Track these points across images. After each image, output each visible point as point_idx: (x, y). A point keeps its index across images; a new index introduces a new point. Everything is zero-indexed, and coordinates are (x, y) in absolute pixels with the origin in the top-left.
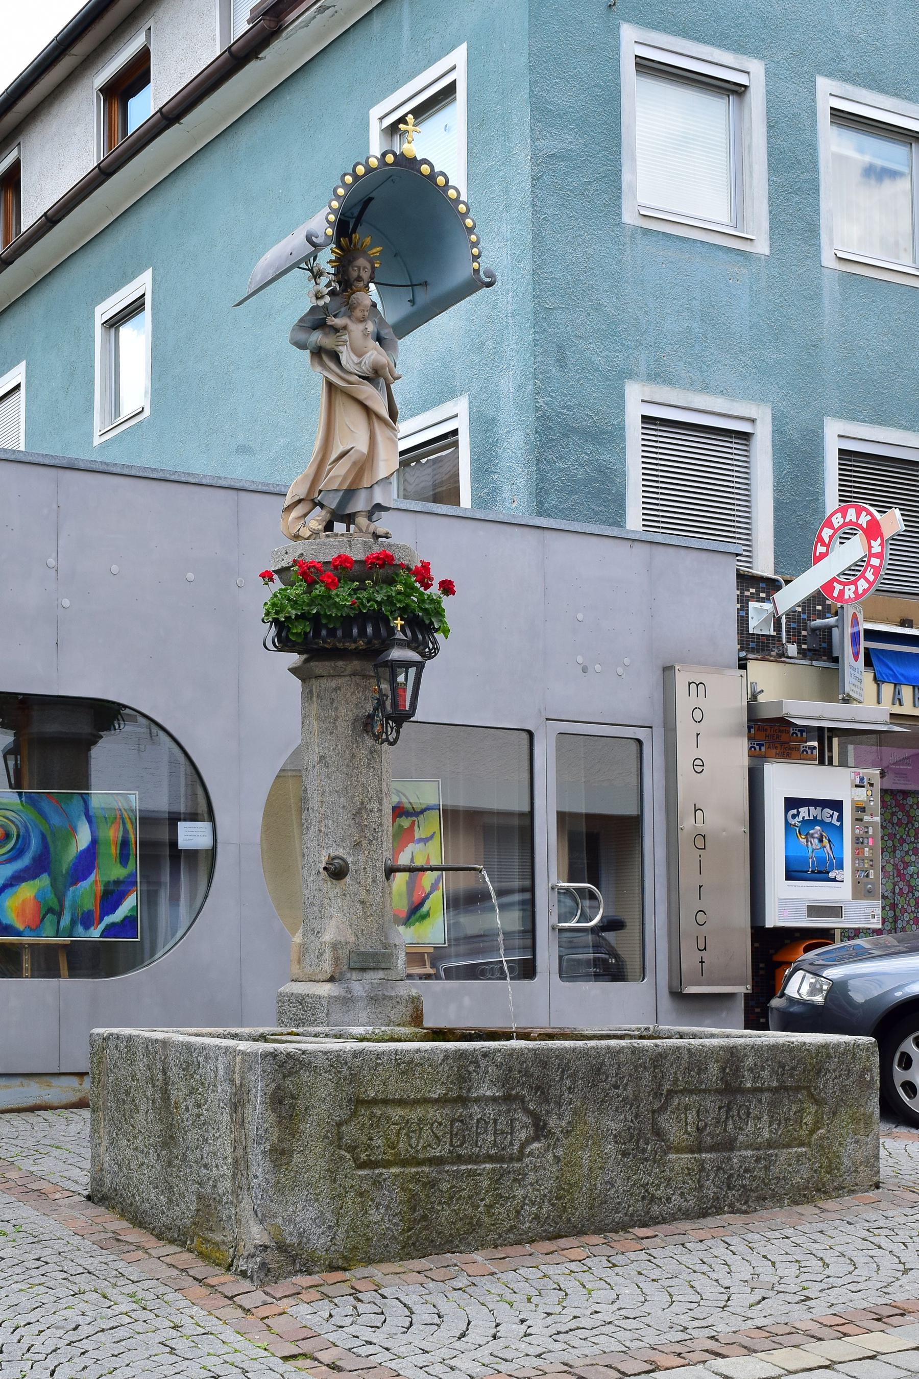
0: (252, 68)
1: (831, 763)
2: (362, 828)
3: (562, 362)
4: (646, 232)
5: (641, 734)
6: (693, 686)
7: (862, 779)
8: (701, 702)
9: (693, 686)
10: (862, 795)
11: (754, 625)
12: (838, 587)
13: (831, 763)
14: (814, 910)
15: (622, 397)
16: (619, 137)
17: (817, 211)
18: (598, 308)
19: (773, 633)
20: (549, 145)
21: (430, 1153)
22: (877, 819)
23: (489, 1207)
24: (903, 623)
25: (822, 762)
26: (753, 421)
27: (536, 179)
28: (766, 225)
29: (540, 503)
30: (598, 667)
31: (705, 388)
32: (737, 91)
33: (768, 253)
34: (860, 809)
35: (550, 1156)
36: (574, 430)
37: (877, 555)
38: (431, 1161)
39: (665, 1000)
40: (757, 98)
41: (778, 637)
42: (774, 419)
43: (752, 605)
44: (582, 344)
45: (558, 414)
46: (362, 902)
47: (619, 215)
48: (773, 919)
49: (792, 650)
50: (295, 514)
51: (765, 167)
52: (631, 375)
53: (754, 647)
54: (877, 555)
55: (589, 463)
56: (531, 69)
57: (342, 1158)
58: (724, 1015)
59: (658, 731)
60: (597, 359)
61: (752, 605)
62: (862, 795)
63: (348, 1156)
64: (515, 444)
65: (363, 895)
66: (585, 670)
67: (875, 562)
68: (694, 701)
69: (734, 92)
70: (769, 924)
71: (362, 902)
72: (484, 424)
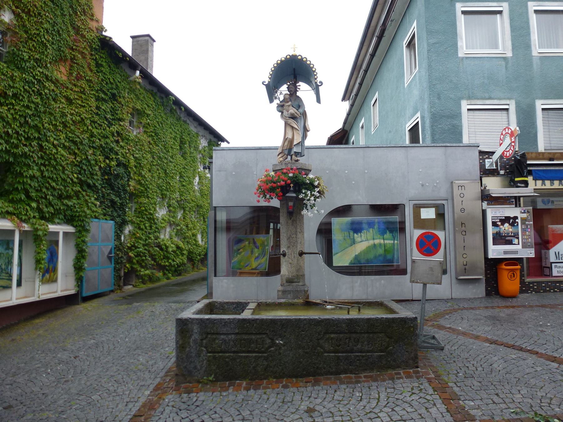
0: (383, 39)
1: (520, 206)
2: (290, 242)
3: (439, 98)
4: (467, 58)
5: (444, 202)
6: (460, 187)
7: (524, 211)
8: (463, 191)
9: (460, 187)
10: (525, 215)
11: (487, 166)
12: (505, 153)
13: (520, 206)
14: (506, 252)
15: (460, 105)
16: (456, 33)
17: (530, 40)
18: (451, 81)
19: (495, 168)
20: (432, 41)
21: (233, 349)
22: (532, 223)
23: (254, 367)
24: (551, 159)
25: (516, 206)
26: (508, 105)
27: (429, 51)
28: (510, 48)
29: (433, 138)
30: (427, 184)
31: (490, 98)
32: (500, 12)
33: (511, 55)
34: (524, 220)
35: (277, 352)
36: (444, 116)
37: (514, 142)
38: (234, 352)
39: (454, 280)
40: (506, 14)
41: (497, 169)
42: (516, 103)
43: (486, 160)
44: (446, 92)
45: (438, 113)
46: (291, 263)
47: (457, 55)
48: (491, 256)
49: (502, 172)
50: (280, 156)
51: (510, 32)
52: (463, 98)
53: (486, 172)
54: (514, 142)
55: (450, 124)
56: (426, 22)
57: (202, 350)
58: (477, 284)
59: (450, 201)
60: (451, 96)
61: (486, 160)
62: (525, 215)
63: (204, 349)
64: (428, 122)
65: (291, 261)
66: (423, 185)
67: (513, 144)
68: (460, 191)
69: (498, 13)
70: (489, 257)
71: (291, 263)
72: (423, 118)
